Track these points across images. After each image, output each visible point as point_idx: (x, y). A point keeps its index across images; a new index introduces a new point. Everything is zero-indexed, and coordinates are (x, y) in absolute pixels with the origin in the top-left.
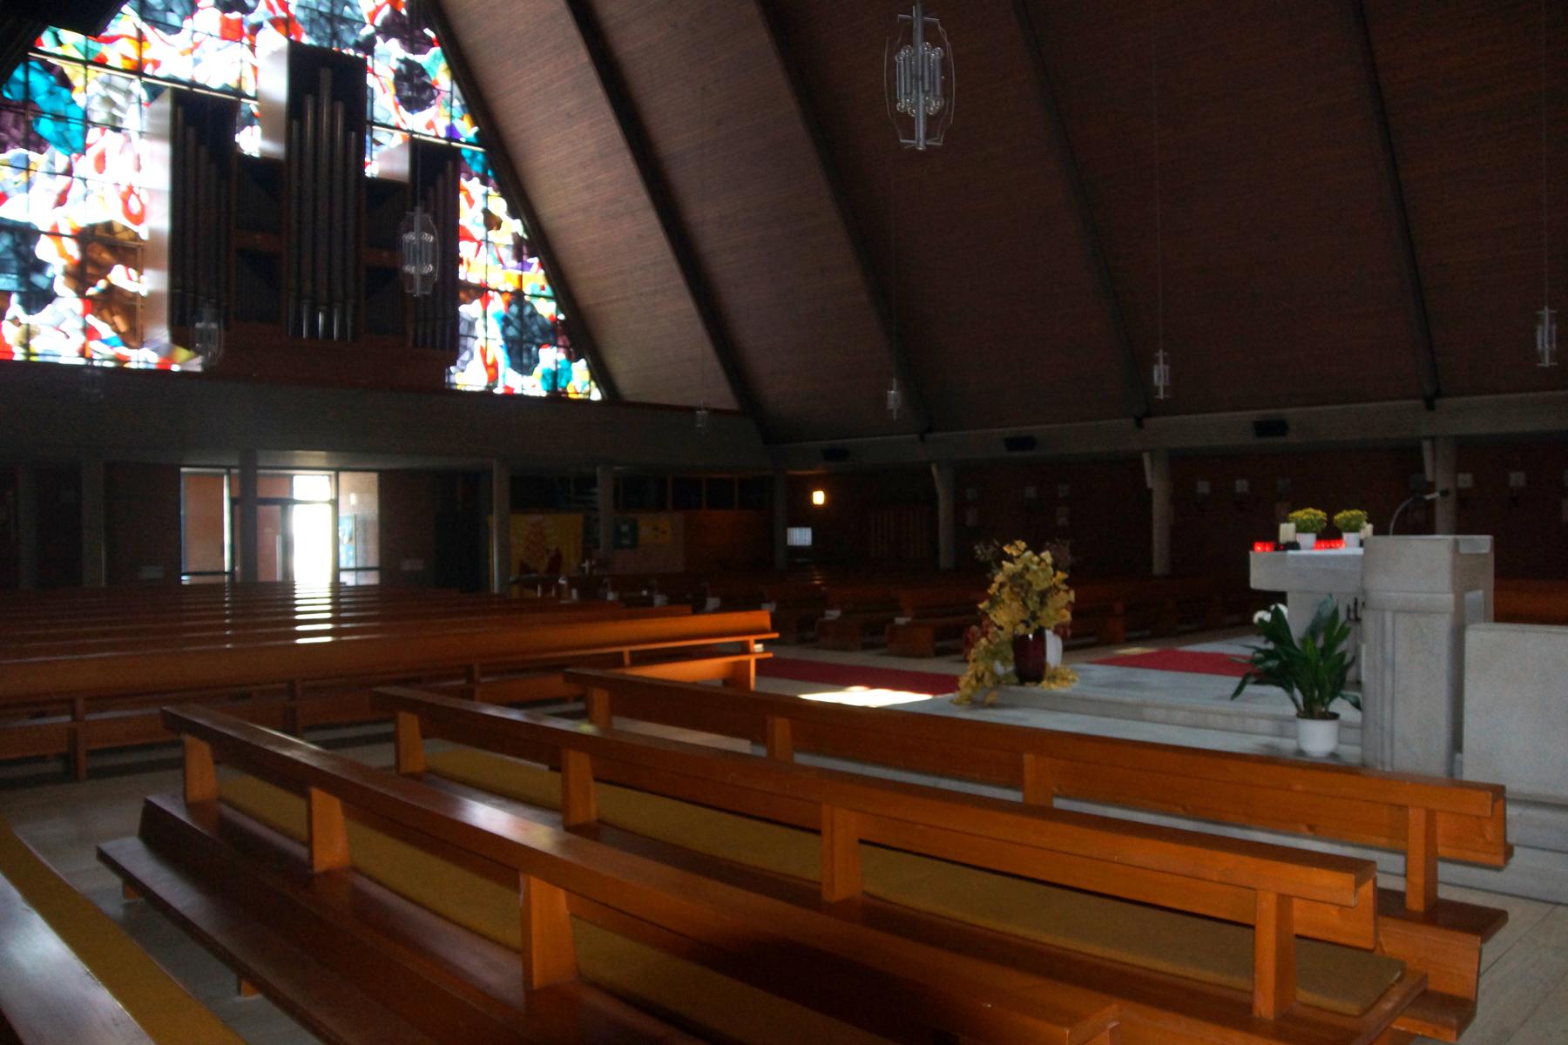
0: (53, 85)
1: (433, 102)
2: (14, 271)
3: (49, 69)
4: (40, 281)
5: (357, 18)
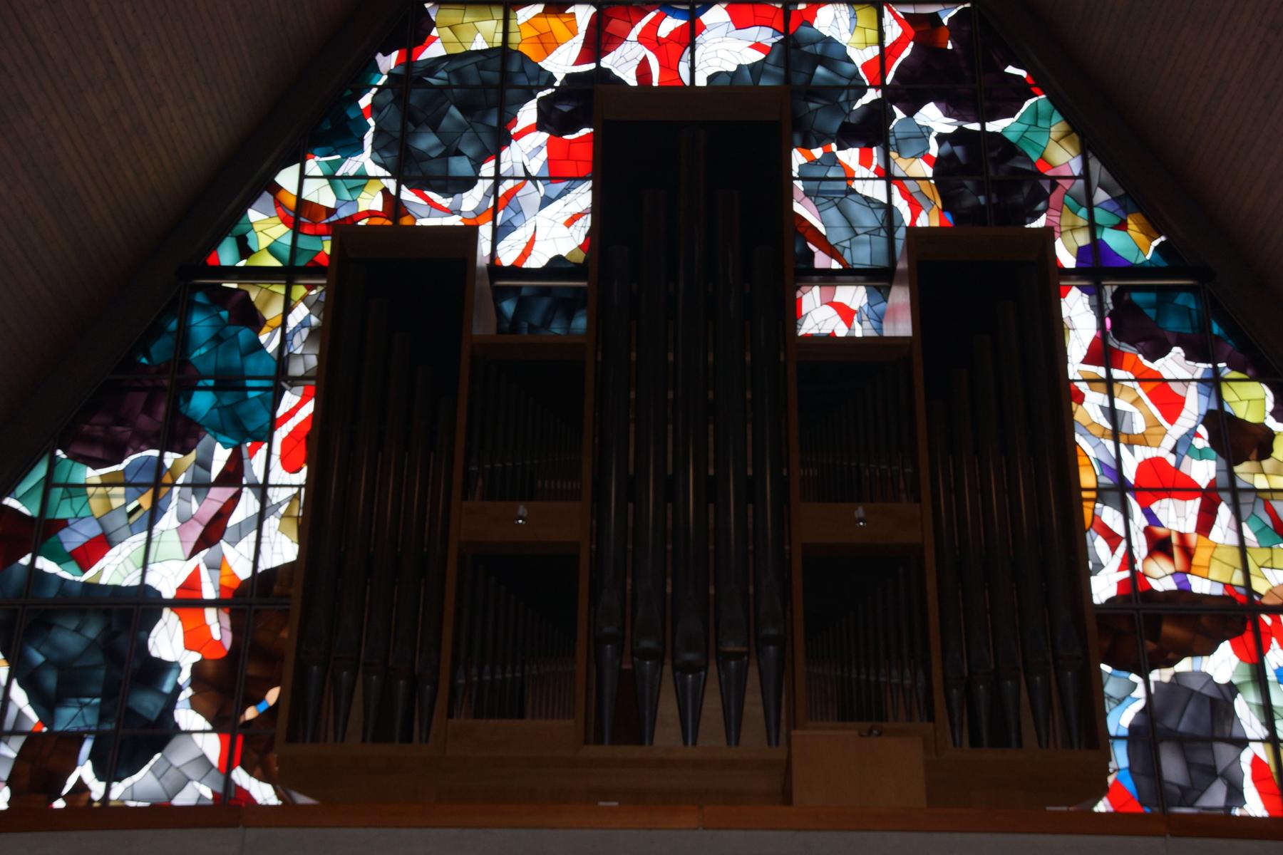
0: (223, 325)
1: (1041, 206)
2: (98, 689)
3: (221, 298)
4: (148, 704)
5: (845, 82)
